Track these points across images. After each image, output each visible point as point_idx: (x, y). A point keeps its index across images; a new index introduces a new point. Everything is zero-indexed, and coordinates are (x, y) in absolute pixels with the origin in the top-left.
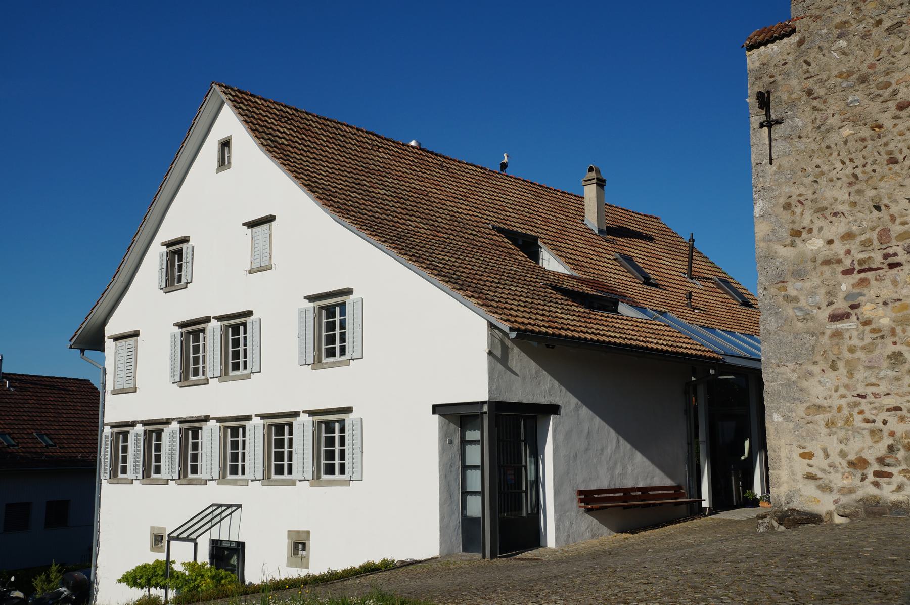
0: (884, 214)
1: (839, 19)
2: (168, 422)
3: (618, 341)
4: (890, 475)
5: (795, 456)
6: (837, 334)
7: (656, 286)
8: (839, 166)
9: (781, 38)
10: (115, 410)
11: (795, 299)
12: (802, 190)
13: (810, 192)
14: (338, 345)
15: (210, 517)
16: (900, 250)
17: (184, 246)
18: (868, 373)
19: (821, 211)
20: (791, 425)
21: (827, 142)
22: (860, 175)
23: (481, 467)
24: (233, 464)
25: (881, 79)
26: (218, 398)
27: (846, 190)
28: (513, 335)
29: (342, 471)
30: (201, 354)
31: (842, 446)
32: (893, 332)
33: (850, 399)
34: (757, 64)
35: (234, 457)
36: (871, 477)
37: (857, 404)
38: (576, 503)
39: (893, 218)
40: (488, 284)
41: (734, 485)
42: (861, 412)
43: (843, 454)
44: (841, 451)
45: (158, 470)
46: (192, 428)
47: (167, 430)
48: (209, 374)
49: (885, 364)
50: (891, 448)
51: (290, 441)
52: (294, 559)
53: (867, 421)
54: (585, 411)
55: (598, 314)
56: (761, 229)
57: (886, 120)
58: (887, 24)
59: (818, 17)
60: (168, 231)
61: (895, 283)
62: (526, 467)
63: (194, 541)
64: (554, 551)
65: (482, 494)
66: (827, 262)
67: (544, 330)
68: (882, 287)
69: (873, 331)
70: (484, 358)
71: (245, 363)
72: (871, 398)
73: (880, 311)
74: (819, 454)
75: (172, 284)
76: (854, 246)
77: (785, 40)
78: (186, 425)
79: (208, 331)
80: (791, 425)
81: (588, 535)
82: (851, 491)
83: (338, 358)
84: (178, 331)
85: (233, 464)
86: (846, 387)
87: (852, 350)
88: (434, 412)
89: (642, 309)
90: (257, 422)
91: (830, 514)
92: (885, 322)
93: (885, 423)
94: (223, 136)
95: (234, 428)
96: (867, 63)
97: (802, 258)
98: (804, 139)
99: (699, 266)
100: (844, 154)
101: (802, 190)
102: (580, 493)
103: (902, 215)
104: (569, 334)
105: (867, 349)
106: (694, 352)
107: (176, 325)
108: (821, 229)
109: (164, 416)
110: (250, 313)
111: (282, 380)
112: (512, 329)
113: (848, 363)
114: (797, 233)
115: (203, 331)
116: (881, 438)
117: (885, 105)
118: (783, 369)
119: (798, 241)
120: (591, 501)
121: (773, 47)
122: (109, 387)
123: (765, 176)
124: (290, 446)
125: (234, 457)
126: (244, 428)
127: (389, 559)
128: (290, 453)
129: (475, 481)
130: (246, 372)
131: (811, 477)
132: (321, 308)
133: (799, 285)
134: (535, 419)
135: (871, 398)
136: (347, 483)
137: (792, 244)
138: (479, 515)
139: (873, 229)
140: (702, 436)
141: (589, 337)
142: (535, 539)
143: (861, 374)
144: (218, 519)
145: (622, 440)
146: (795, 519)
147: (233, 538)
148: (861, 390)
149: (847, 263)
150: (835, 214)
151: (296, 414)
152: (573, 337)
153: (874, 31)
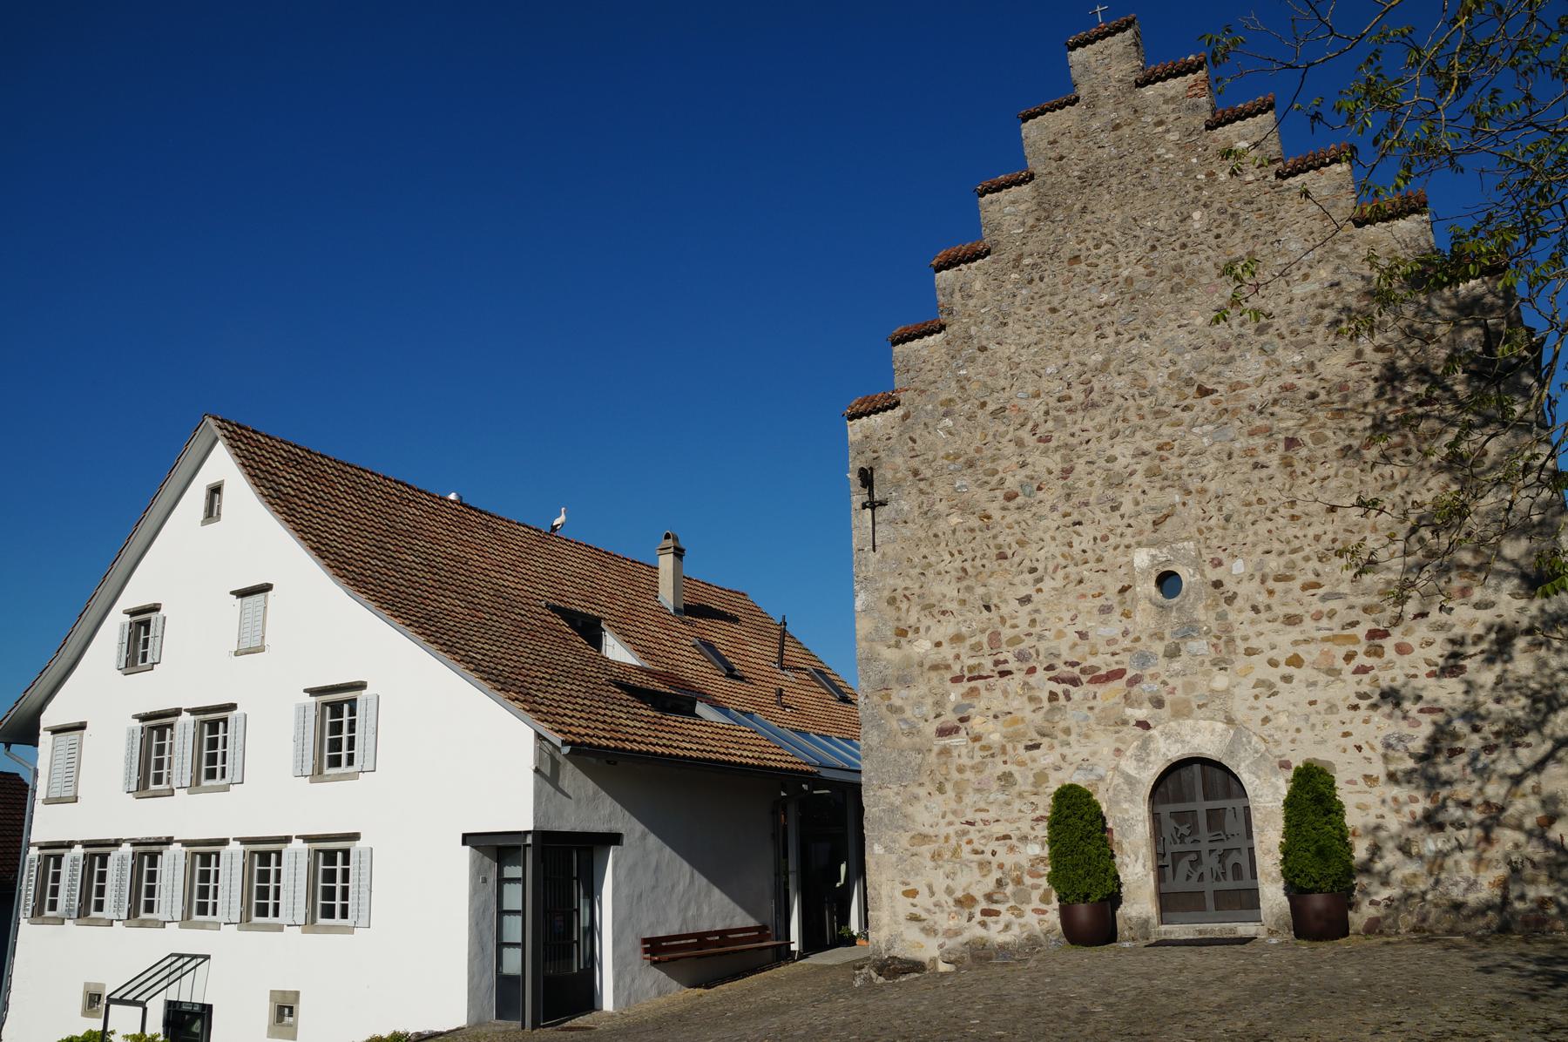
0: (994, 614)
1: (944, 396)
2: (117, 843)
3: (694, 754)
4: (997, 913)
5: (898, 894)
6: (945, 752)
7: (742, 679)
8: (947, 557)
9: (885, 409)
10: (45, 824)
11: (900, 710)
12: (908, 583)
13: (917, 586)
14: (344, 753)
15: (167, 972)
16: (1010, 657)
17: (153, 616)
18: (978, 796)
19: (927, 608)
20: (894, 858)
21: (935, 530)
22: (969, 570)
23: (523, 913)
24: (201, 902)
25: (988, 466)
26: (185, 815)
27: (955, 585)
28: (566, 750)
29: (344, 915)
30: (166, 757)
31: (949, 882)
32: (1004, 750)
33: (958, 827)
34: (859, 436)
35: (204, 892)
36: (978, 917)
37: (965, 833)
38: (639, 953)
39: (1003, 620)
40: (537, 681)
41: (828, 925)
42: (970, 842)
43: (949, 891)
44: (948, 888)
45: (100, 906)
46: (148, 852)
47: (115, 855)
48: (175, 783)
49: (995, 785)
50: (999, 883)
51: (278, 873)
52: (278, 1028)
53: (976, 852)
54: (652, 839)
55: (672, 719)
56: (863, 626)
57: (994, 510)
58: (991, 407)
59: (923, 391)
60: (133, 597)
61: (1005, 693)
62: (578, 911)
63: (142, 1004)
64: (612, 1016)
65: (523, 945)
66: (935, 667)
67: (604, 742)
68: (992, 698)
69: (983, 748)
70: (530, 776)
71: (224, 770)
72: (980, 825)
73: (991, 725)
74: (924, 891)
75: (134, 664)
76: (964, 649)
77: (889, 412)
78: (141, 849)
79: (176, 727)
80: (894, 858)
81: (653, 993)
82: (957, 933)
83: (344, 769)
84: (138, 724)
85: (201, 902)
86: (954, 812)
87: (961, 770)
88: (464, 843)
89: (723, 710)
90: (235, 847)
91: (934, 960)
92: (995, 738)
93: (994, 853)
94: (213, 480)
95: (205, 854)
96: (973, 446)
97: (907, 663)
98: (910, 525)
99: (792, 654)
100: (952, 545)
101: (908, 583)
102: (645, 941)
103: (1012, 618)
104: (636, 747)
105: (978, 769)
106: (785, 765)
107: (135, 717)
108: (928, 628)
109: (111, 835)
110: (233, 707)
111: (273, 793)
112: (564, 743)
113: (956, 784)
114: (902, 633)
115: (171, 726)
116: (990, 871)
117: (992, 494)
118: (886, 792)
119: (903, 641)
120: (657, 950)
121: (876, 419)
122: (41, 793)
123: (868, 564)
124: (278, 880)
125: (204, 892)
126: (218, 855)
127: (401, 1030)
128: (277, 890)
129: (514, 929)
130: (223, 782)
131: (914, 918)
132: (325, 704)
133: (904, 693)
134: (591, 850)
135: (980, 825)
136: (349, 930)
137: (897, 645)
138: (518, 972)
139: (983, 631)
140: (793, 864)
141: (659, 750)
142: (587, 999)
143: (970, 798)
144: (178, 973)
145: (696, 874)
146: (896, 968)
147: (197, 999)
148: (969, 817)
149: (956, 669)
150: (944, 613)
151: (287, 840)
152: (640, 751)
153: (980, 412)
